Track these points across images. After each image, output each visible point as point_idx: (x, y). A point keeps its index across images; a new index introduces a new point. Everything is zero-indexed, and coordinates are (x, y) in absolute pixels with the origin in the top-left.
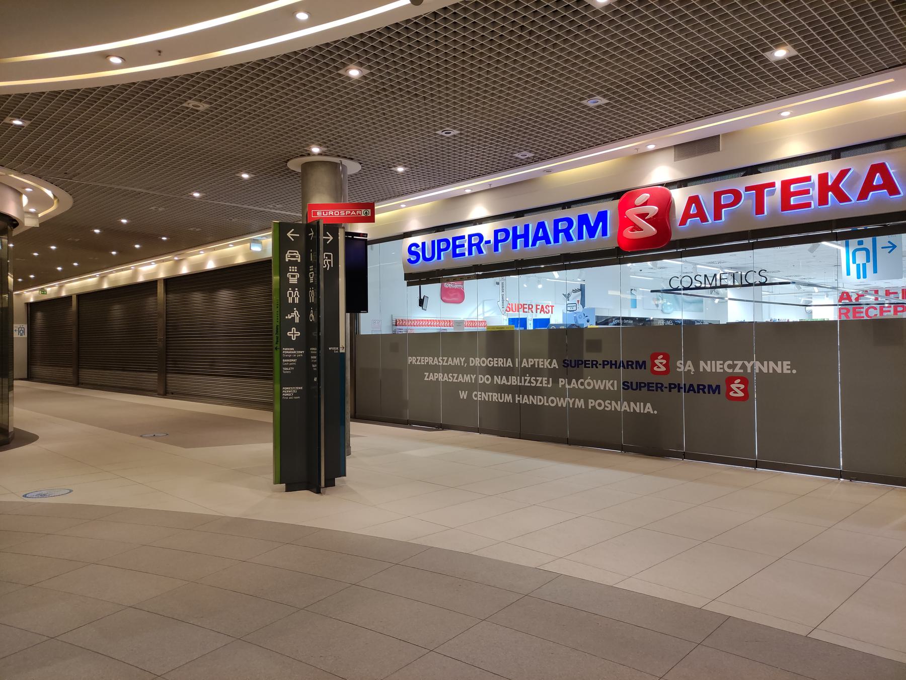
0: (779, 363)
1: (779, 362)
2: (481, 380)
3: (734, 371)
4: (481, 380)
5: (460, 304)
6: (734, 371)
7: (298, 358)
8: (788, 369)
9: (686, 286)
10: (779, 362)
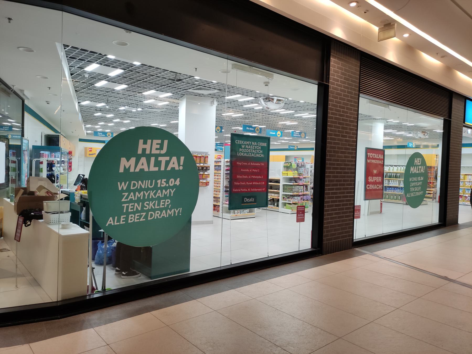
0: (149, 141)
1: (160, 140)
2: (246, 200)
3: (135, 171)
4: (246, 200)
5: (415, 209)
6: (135, 171)
7: (170, 197)
8: (157, 149)
9: (18, 266)
10: (160, 140)
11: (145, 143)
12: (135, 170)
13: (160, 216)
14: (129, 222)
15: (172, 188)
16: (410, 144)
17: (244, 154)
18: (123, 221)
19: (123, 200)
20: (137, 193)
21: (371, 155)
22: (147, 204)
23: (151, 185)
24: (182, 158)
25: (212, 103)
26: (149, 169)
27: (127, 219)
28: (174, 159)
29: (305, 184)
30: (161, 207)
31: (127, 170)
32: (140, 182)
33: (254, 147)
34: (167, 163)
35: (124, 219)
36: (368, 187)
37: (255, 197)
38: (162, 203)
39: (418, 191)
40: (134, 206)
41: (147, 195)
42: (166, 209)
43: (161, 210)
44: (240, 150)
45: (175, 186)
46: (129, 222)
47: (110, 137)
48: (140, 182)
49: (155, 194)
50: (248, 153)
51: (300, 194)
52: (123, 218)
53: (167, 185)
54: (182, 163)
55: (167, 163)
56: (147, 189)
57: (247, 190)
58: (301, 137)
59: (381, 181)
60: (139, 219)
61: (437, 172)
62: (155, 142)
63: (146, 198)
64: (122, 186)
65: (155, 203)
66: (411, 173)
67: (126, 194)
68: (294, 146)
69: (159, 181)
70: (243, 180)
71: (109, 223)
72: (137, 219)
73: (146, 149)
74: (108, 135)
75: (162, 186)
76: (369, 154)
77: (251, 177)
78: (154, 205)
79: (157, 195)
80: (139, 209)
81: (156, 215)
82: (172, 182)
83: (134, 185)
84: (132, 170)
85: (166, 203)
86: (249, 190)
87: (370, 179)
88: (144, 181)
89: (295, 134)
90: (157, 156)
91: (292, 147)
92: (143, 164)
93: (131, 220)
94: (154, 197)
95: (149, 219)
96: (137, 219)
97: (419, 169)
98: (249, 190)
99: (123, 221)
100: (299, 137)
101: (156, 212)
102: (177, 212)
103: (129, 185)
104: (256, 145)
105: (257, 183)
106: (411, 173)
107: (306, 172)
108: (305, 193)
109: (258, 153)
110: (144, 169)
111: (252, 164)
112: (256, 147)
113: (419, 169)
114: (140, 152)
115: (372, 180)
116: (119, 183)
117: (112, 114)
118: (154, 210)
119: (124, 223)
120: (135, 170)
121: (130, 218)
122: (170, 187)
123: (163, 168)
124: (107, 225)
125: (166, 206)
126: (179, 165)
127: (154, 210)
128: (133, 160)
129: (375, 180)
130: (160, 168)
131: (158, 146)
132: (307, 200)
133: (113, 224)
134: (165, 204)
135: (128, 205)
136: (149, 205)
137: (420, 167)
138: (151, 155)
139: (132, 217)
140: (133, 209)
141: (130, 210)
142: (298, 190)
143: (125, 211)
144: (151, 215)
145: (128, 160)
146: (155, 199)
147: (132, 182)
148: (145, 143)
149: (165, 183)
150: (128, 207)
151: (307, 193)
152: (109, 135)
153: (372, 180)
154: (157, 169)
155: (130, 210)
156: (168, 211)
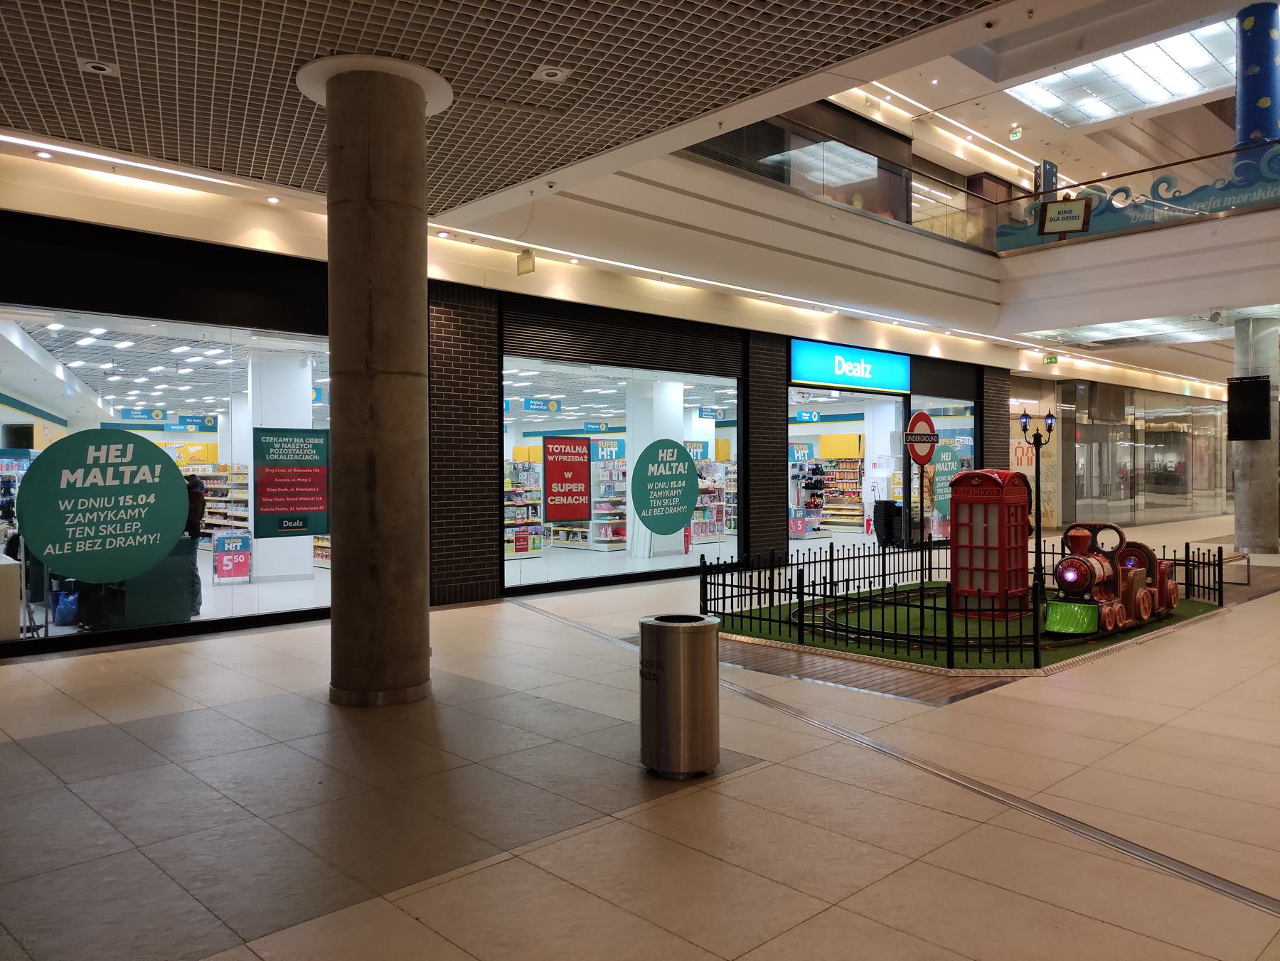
0: (104, 448)
1: (122, 445)
8: (116, 457)
10: (122, 445)
11: (98, 449)
12: (83, 484)
13: (124, 543)
14: (77, 550)
15: (143, 507)
16: (804, 414)
17: (279, 457)
18: (68, 550)
19: (67, 523)
20: (88, 514)
21: (557, 449)
22: (103, 528)
23: (109, 503)
24: (158, 468)
25: (304, 365)
26: (105, 482)
27: (74, 546)
28: (145, 468)
29: (531, 502)
30: (126, 531)
31: (71, 485)
32: (91, 500)
33: (299, 446)
34: (134, 474)
35: (69, 547)
36: (552, 500)
37: (305, 520)
38: (126, 527)
39: (673, 506)
40: (83, 530)
41: (102, 516)
42: (134, 535)
43: (126, 536)
44: (272, 450)
45: (147, 504)
46: (77, 550)
47: (161, 419)
48: (91, 500)
49: (116, 515)
50: (287, 455)
51: (519, 522)
52: (68, 545)
53: (135, 503)
54: (157, 474)
55: (134, 474)
56: (103, 509)
57: (289, 509)
58: (548, 410)
59: (583, 491)
60: (92, 547)
61: (863, 469)
62: (113, 447)
63: (102, 520)
64: (65, 505)
65: (116, 526)
66: (649, 474)
67: (72, 515)
68: (599, 424)
69: (121, 499)
70: (278, 495)
71: (47, 551)
72: (89, 547)
73: (99, 457)
74: (154, 416)
75: (126, 504)
76: (550, 446)
77: (295, 489)
78: (115, 529)
79: (119, 516)
80: (92, 534)
81: (118, 542)
82: (142, 499)
83: (83, 504)
84: (79, 485)
85: (134, 528)
86: (291, 509)
87: (555, 487)
88: (98, 499)
89: (533, 404)
90: (116, 466)
91: (593, 427)
92: (95, 477)
93: (80, 548)
94: (114, 519)
95: (107, 547)
96: (89, 547)
97: (948, 465)
98: (291, 509)
99: (68, 550)
100: (545, 410)
101: (119, 538)
102: (152, 539)
103: (76, 503)
104: (301, 443)
105: (307, 499)
106: (649, 474)
107: (532, 481)
108: (530, 521)
109: (307, 454)
110: (97, 483)
111: (295, 470)
112: (302, 446)
113: (948, 465)
114: (90, 461)
115: (562, 488)
116: (60, 502)
117: (146, 377)
118: (116, 537)
119: (70, 551)
120: (83, 484)
121: (78, 546)
122: (139, 506)
123: (126, 481)
124: (45, 554)
125: (133, 531)
126: (153, 477)
127: (116, 537)
128: (80, 472)
129: (570, 488)
130: (122, 482)
131: (119, 453)
132: (536, 534)
133: (53, 553)
134: (132, 527)
135: (74, 529)
136: (106, 529)
137: (949, 463)
138: (107, 465)
139: (80, 544)
140: (83, 534)
141: (77, 536)
142: (513, 515)
143: (70, 537)
144: (111, 543)
145: (73, 472)
146: (116, 522)
147: (80, 500)
148: (98, 449)
149: (131, 502)
150: (74, 532)
151: (536, 520)
152: (157, 416)
153: (562, 488)
154: (117, 482)
155: (77, 536)
156: (138, 537)
